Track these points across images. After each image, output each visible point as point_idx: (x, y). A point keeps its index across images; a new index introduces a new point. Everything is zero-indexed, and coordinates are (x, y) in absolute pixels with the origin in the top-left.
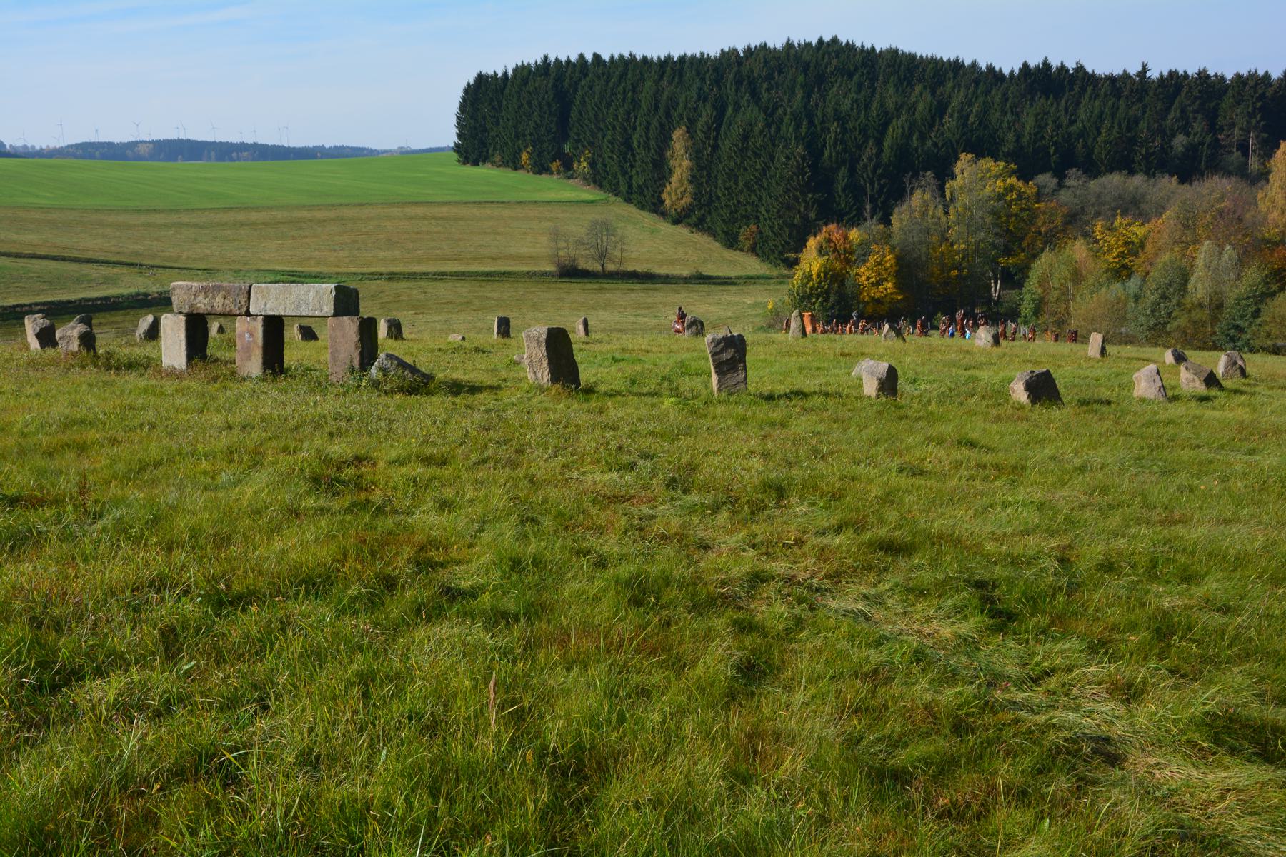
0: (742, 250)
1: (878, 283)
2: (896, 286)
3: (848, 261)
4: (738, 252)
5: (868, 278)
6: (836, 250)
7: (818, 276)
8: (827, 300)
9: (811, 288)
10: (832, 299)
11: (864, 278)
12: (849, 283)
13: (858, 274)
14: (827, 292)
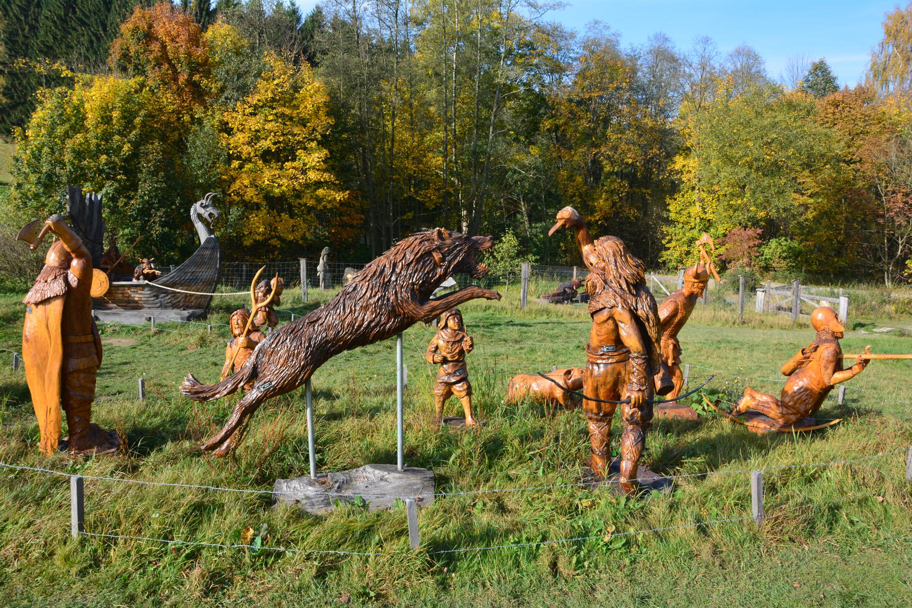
1: (280, 155)
2: (330, 164)
3: (198, 93)
5: (256, 138)
6: (164, 58)
7: (107, 120)
10: (145, 187)
11: (240, 138)
12: (197, 145)
13: (226, 129)
14: (130, 167)
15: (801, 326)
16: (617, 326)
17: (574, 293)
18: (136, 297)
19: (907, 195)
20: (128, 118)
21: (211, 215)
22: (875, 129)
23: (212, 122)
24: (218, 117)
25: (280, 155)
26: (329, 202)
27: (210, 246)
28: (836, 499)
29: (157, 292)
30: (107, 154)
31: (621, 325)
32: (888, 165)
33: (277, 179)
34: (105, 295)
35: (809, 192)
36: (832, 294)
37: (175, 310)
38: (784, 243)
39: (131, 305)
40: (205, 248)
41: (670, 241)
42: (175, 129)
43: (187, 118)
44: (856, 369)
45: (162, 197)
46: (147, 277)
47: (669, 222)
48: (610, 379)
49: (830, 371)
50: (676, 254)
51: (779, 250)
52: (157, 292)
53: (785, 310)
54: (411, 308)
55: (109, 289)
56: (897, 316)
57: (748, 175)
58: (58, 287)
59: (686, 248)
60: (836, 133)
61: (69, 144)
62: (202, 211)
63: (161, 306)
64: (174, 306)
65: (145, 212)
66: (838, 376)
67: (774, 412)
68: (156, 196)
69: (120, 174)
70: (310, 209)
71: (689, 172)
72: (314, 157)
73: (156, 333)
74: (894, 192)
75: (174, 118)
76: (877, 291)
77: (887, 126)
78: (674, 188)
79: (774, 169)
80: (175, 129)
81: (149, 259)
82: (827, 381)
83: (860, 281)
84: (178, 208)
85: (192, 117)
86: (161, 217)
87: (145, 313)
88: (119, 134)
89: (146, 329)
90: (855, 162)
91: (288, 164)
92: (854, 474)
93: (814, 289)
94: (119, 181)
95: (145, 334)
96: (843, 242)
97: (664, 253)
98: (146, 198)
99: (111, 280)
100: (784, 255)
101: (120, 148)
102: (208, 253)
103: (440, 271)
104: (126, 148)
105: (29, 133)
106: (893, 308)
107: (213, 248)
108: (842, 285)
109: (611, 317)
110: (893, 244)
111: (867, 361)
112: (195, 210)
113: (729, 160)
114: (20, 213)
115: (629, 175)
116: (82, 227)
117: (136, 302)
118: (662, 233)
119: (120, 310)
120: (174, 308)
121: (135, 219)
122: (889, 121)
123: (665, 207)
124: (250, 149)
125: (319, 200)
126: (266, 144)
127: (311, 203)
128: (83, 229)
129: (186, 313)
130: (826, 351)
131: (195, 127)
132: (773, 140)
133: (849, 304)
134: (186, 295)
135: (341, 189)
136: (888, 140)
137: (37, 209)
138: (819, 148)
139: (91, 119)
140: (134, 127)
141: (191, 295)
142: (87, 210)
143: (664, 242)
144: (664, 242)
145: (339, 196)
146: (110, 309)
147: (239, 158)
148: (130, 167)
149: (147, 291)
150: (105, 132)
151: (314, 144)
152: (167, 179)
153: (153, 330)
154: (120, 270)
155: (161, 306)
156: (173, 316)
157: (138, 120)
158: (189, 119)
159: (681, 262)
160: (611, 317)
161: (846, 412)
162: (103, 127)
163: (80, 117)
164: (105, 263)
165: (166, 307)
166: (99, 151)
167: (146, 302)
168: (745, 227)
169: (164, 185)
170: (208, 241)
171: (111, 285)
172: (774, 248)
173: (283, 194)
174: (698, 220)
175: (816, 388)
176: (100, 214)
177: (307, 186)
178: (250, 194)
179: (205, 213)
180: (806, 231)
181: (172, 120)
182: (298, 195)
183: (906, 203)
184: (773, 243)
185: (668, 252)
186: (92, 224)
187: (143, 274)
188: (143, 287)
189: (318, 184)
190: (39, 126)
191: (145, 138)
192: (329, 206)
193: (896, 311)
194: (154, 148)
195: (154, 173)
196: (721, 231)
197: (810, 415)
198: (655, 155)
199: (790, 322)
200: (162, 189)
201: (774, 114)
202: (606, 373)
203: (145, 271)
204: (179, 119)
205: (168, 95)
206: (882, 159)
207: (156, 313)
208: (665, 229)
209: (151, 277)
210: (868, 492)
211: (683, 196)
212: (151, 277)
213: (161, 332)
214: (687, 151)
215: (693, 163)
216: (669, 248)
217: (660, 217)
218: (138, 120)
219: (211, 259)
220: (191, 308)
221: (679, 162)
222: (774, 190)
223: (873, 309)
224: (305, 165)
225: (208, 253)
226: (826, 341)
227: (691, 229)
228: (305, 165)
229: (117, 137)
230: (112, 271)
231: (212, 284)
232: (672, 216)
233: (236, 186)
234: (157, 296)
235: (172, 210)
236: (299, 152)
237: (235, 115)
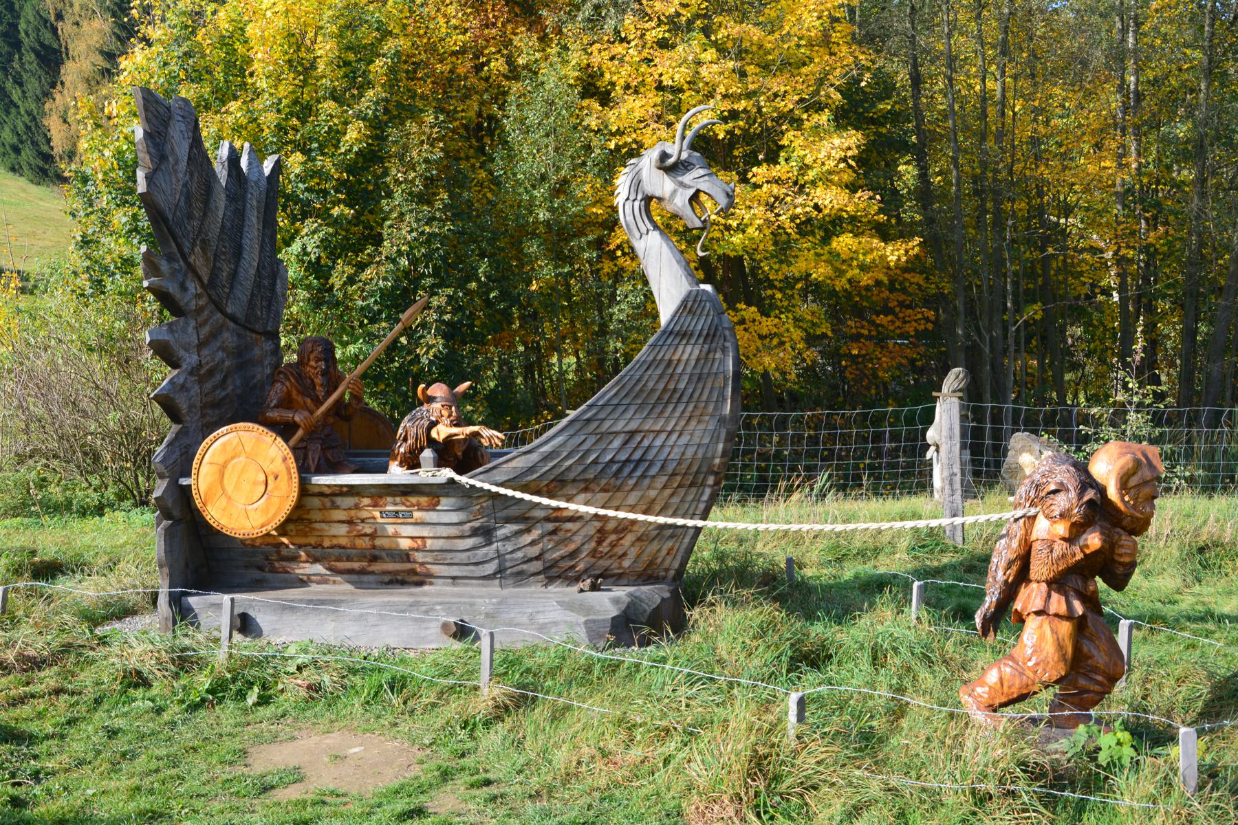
10: (402, 230)
13: (593, 88)
14: (363, 181)
18: (404, 535)
20: (353, 78)
23: (559, 74)
24: (575, 57)
26: (863, 268)
27: (700, 325)
30: (306, 152)
34: (282, 529)
37: (557, 589)
39: (394, 572)
40: (677, 333)
43: (497, 65)
45: (444, 258)
46: (447, 453)
52: (490, 516)
55: (299, 506)
62: (662, 185)
63: (500, 573)
64: (555, 572)
65: (398, 298)
68: (428, 257)
69: (337, 202)
72: (829, 148)
73: (500, 712)
75: (465, 66)
81: (452, 385)
84: (484, 289)
85: (510, 61)
86: (441, 310)
87: (442, 600)
88: (335, 99)
89: (456, 683)
91: (760, 173)
94: (335, 222)
95: (451, 710)
98: (404, 262)
99: (304, 470)
101: (335, 136)
102: (689, 353)
104: (352, 134)
112: (637, 184)
114: (90, 313)
116: (197, 259)
117: (405, 556)
119: (342, 587)
120: (551, 580)
126: (702, 116)
128: (205, 274)
129: (607, 602)
134: (603, 529)
139: (264, 59)
140: (369, 84)
141: (624, 527)
142: (220, 202)
145: (894, 253)
146: (303, 582)
148: (363, 181)
149: (447, 514)
151: (824, 118)
152: (457, 211)
153: (490, 692)
154: (338, 435)
155: (500, 573)
156: (556, 619)
158: (504, 69)
163: (238, 68)
164: (287, 403)
165: (521, 577)
169: (449, 226)
170: (689, 306)
171: (305, 490)
176: (271, 242)
177: (805, 226)
181: (461, 70)
186: (238, 253)
187: (432, 443)
188: (433, 493)
189: (833, 225)
191: (397, 111)
194: (421, 142)
195: (424, 198)
200: (443, 239)
203: (442, 432)
204: (478, 68)
205: (451, 10)
207: (479, 600)
209: (462, 456)
212: (462, 456)
213: (523, 700)
218: (378, 67)
219: (699, 379)
220: (618, 578)
228: (804, 168)
229: (329, 106)
230: (311, 435)
234: (486, 533)
235: (468, 293)
236: (789, 137)
237: (619, 49)
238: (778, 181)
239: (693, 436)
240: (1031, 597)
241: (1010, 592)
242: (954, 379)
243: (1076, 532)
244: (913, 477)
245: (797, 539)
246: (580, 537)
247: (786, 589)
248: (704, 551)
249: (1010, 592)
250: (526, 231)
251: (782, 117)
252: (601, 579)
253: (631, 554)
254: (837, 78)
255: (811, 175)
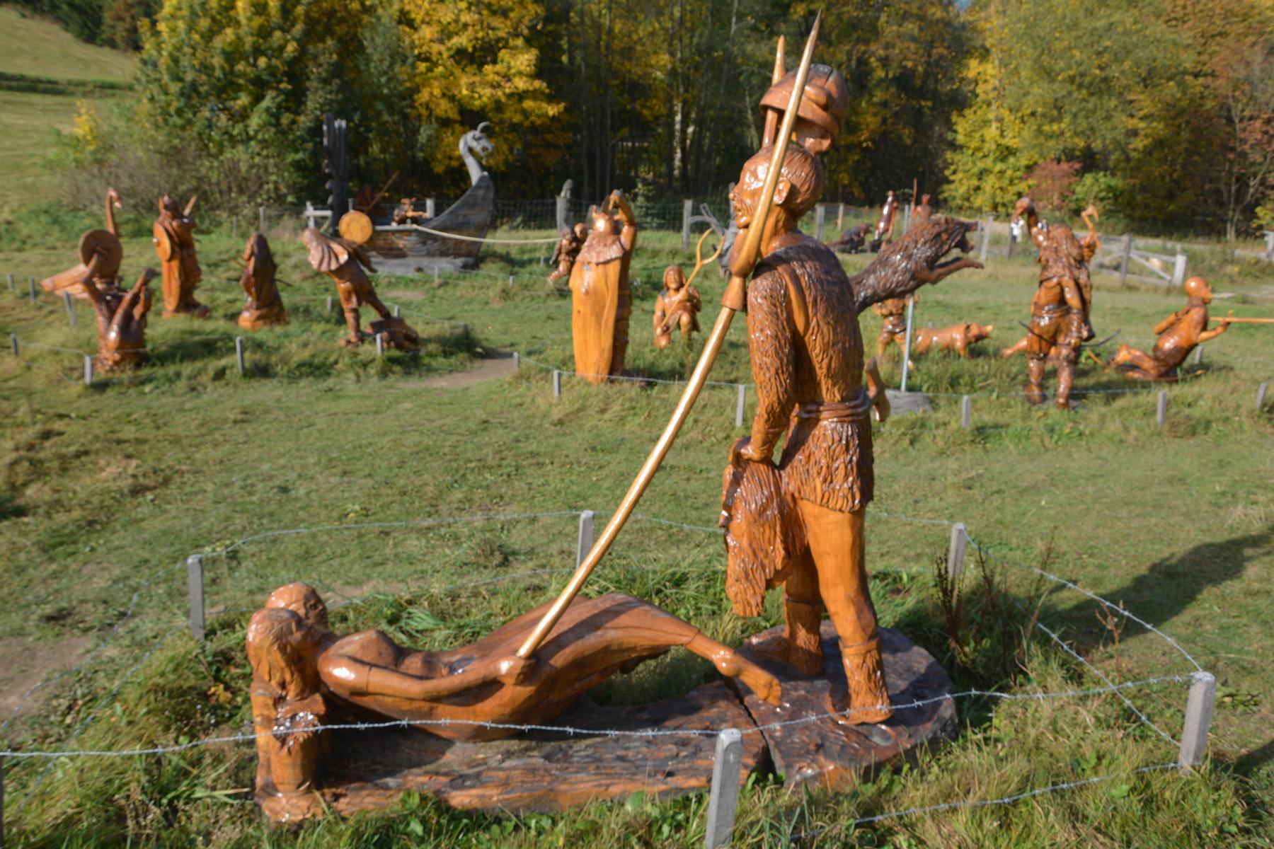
0: (112, 44)
1: (479, 56)
4: (107, 50)
5: (446, 34)
8: (295, 100)
9: (231, 56)
10: (315, 100)
11: (427, 32)
14: (296, 72)
15: (1131, 288)
16: (1062, 291)
17: (862, 242)
19: (1268, 121)
21: (484, 149)
22: (1240, 28)
25: (479, 56)
26: (539, 116)
27: (484, 184)
28: (1208, 416)
29: (425, 238)
31: (1067, 289)
32: (1248, 80)
33: (477, 88)
35: (1141, 114)
36: (1164, 251)
37: (449, 259)
38: (1102, 180)
40: (478, 187)
41: (954, 172)
42: (342, 20)
44: (1220, 329)
47: (954, 146)
48: (1052, 329)
49: (1198, 330)
50: (962, 190)
51: (1096, 189)
53: (1108, 268)
54: (926, 273)
56: (1240, 279)
57: (1070, 93)
58: (614, 252)
59: (975, 182)
60: (1186, 36)
61: (218, 42)
62: (474, 144)
64: (444, 254)
66: (1204, 335)
67: (1148, 364)
70: (514, 128)
71: (986, 81)
72: (524, 60)
73: (441, 286)
74: (1251, 118)
76: (1219, 248)
77: (1254, 25)
78: (960, 102)
79: (1102, 87)
80: (342, 20)
82: (1194, 339)
83: (1197, 235)
87: (413, 262)
90: (1205, 75)
92: (1220, 402)
93: (1141, 242)
96: (1182, 184)
97: (945, 187)
99: (374, 223)
100: (1103, 194)
101: (282, 48)
102: (481, 192)
103: (946, 247)
105: (162, 27)
106: (1236, 269)
107: (487, 188)
108: (1180, 239)
109: (1059, 284)
110: (1242, 182)
111: (1228, 324)
112: (466, 143)
113: (1048, 74)
115: (903, 81)
117: (400, 249)
118: (945, 161)
121: (304, 141)
122: (1258, 18)
123: (950, 126)
124: (442, 48)
125: (526, 114)
126: (462, 40)
127: (517, 119)
129: (460, 261)
130: (1196, 314)
131: (366, 19)
132: (1106, 48)
133: (1187, 263)
134: (457, 241)
135: (550, 99)
136: (1254, 44)
137: (183, 128)
138: (1163, 58)
141: (463, 241)
143: (947, 173)
144: (947, 173)
145: (552, 110)
147: (427, 59)
148: (296, 72)
149: (414, 238)
150: (261, 27)
157: (300, 10)
159: (968, 199)
160: (1059, 284)
161: (1205, 367)
162: (258, 21)
166: (257, 52)
167: (411, 249)
168: (1059, 161)
170: (482, 179)
171: (374, 231)
172: (1091, 184)
173: (483, 108)
174: (994, 147)
175: (1185, 344)
178: (444, 108)
179: (477, 147)
180: (1130, 166)
182: (499, 106)
183: (1266, 133)
184: (1088, 179)
185: (952, 186)
188: (409, 232)
190: (173, 16)
192: (538, 122)
193: (1240, 274)
196: (1024, 162)
197: (1173, 367)
198: (941, 57)
199: (1118, 284)
201: (1109, 12)
202: (1050, 325)
206: (1241, 73)
207: (425, 262)
208: (949, 155)
210: (1229, 414)
211: (975, 112)
214: (985, 54)
215: (990, 69)
216: (953, 182)
217: (942, 138)
221: (973, 68)
222: (1100, 114)
223: (1212, 269)
224: (509, 68)
225: (481, 192)
226: (1197, 306)
227: (984, 156)
229: (278, 34)
231: (483, 229)
232: (961, 139)
233: (424, 96)
234: (424, 243)
238: (497, 73)
239: (480, 216)
240: (562, 257)
241: (558, 256)
242: (568, 185)
243: (571, 243)
244: (553, 225)
245: (508, 245)
246: (451, 244)
247: (509, 262)
248: (482, 249)
249: (558, 256)
250: (377, 96)
251: (499, 40)
252: (457, 255)
253: (464, 249)
254: (526, 21)
255: (513, 71)
